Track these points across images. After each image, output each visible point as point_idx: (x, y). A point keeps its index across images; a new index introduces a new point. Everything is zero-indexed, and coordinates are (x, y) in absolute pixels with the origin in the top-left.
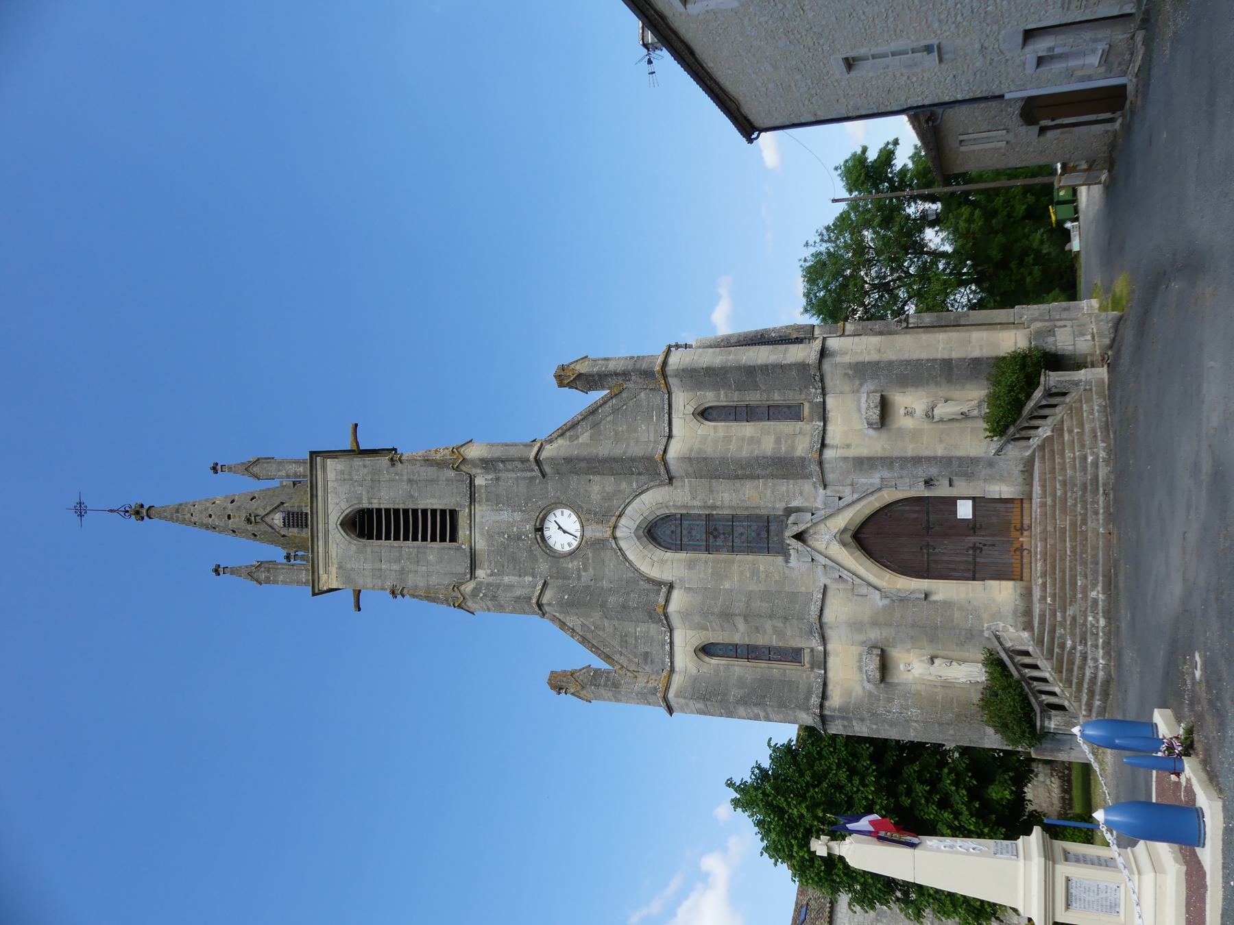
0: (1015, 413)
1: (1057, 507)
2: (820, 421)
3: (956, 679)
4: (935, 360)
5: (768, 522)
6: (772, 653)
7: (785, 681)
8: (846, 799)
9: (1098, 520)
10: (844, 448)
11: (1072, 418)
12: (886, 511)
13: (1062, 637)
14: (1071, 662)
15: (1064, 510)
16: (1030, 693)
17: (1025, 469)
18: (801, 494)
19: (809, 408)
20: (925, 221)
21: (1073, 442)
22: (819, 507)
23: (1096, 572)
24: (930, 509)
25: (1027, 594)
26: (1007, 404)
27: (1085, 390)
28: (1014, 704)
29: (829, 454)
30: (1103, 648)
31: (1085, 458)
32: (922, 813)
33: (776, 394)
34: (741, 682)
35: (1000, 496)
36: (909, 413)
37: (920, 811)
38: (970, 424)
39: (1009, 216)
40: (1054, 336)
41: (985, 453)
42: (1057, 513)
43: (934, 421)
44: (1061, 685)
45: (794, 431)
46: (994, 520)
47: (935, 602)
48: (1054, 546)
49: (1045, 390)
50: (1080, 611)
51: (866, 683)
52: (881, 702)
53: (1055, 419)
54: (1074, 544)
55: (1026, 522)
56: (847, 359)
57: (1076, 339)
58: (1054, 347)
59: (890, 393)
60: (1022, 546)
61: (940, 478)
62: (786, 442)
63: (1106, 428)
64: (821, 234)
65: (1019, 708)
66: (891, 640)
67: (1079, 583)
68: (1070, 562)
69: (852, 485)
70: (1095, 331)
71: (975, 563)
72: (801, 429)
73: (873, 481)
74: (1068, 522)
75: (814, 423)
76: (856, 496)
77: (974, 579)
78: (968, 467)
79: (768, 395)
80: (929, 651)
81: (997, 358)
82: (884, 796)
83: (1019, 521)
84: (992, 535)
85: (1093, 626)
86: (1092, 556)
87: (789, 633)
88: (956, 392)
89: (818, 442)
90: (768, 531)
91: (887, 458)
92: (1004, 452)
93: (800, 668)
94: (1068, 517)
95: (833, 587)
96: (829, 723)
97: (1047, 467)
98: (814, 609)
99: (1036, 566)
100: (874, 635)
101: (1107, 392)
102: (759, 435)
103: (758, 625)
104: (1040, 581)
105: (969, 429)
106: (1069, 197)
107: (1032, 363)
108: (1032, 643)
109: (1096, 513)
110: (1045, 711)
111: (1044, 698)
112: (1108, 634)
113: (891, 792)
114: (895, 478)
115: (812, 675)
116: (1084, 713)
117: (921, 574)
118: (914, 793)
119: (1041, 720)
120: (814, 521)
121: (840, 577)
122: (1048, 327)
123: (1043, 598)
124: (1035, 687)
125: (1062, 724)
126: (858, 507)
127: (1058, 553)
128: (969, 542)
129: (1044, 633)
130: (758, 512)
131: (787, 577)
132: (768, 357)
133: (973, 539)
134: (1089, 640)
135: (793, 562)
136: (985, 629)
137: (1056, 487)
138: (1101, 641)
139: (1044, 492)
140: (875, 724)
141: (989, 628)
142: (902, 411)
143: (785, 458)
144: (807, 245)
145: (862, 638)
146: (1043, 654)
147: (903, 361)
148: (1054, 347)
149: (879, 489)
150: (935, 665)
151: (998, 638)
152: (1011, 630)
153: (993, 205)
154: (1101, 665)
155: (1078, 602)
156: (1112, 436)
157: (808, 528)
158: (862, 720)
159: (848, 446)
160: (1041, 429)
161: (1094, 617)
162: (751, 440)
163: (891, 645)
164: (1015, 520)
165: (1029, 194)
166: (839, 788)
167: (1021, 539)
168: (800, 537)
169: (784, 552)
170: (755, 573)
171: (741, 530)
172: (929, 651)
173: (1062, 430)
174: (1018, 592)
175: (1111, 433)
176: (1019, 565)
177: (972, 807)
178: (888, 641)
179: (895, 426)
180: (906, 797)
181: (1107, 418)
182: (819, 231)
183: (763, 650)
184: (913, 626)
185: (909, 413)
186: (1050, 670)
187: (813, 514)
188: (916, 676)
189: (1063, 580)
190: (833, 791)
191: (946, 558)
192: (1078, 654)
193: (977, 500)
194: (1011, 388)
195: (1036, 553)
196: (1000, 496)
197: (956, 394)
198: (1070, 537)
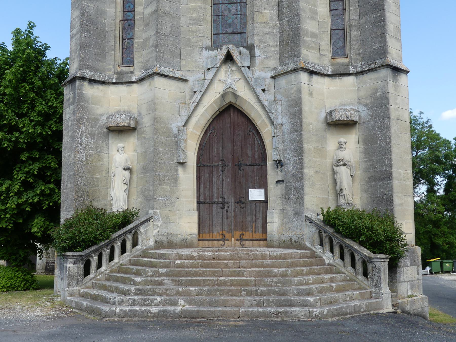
0: (347, 233)
1: (263, 269)
2: (332, 72)
3: (113, 189)
4: (390, 165)
5: (241, 33)
6: (129, 41)
7: (105, 50)
8: (24, 112)
9: (252, 306)
10: (309, 90)
11: (343, 281)
12: (253, 131)
13: (146, 273)
14: (123, 281)
15: (259, 275)
16: (98, 246)
17: (293, 242)
18: (267, 58)
19: (343, 63)
20: (432, 185)
21: (323, 283)
22: (256, 74)
23: (202, 304)
24: (256, 167)
25: (186, 244)
26: (356, 226)
27: (371, 292)
28: (87, 234)
29: (304, 76)
30: (130, 310)
31: (310, 294)
32: (17, 169)
33: (356, 33)
34: (101, 13)
35: (269, 222)
36: (341, 146)
37: (20, 168)
38: (331, 197)
39: (435, 235)
40: (411, 265)
41: (307, 209)
42: (257, 269)
43: (335, 168)
44: (108, 271)
45: (323, 50)
46: (248, 218)
47: (177, 171)
48: (227, 266)
49: (371, 258)
50: (167, 289)
51: (105, 117)
52: (90, 129)
53: (341, 267)
54: (229, 284)
55: (247, 243)
56: (391, 90)
57: (408, 283)
58: (402, 264)
59: (358, 131)
60: (227, 240)
61: (284, 173)
62: (313, 42)
63: (340, 313)
64: (427, 122)
65: (84, 237)
66: (143, 136)
67: (192, 289)
68: (212, 281)
69: (275, 100)
70: (415, 298)
71: (212, 203)
72: (325, 55)
73: (280, 117)
74: (248, 278)
75: (330, 67)
76: (266, 103)
77: (198, 203)
78: (294, 195)
79: (355, 26)
80: (136, 167)
81: (393, 217)
82: (27, 140)
83: (248, 238)
84: (235, 216)
85: (152, 301)
86: (217, 301)
87: (146, 52)
88: (359, 185)
89: (314, 69)
90: (233, 33)
91: (301, 126)
92: (309, 224)
93: (117, 63)
94: (254, 278)
95: (186, 87)
96: (71, 87)
97: (297, 260)
98: (166, 70)
99: (209, 251)
100: (146, 121)
101: (372, 312)
102: (318, 20)
103: (151, 24)
104: (195, 254)
105: (326, 197)
106: (445, 269)
107: (393, 247)
108: (145, 248)
109: (259, 305)
110: (82, 259)
111: (94, 258)
112: (143, 315)
113: (31, 146)
114: (283, 135)
115: (111, 73)
116: (82, 291)
117: (201, 160)
118: (32, 163)
119: (73, 256)
120: (243, 69)
121: (195, 92)
122: (418, 259)
123: (180, 257)
124: (105, 251)
125: (71, 273)
126: (257, 106)
127: (220, 269)
128: (228, 198)
129: (152, 258)
130: (250, 22)
131: (193, 49)
132: (392, 23)
133: (231, 201)
134: (140, 297)
135: (207, 54)
136: (155, 210)
137: (280, 267)
138: (137, 309)
139: (276, 258)
140: (71, 124)
141: (155, 213)
142: (343, 140)
143: (299, 40)
144: (421, 113)
145: (144, 112)
146: (135, 257)
147: (390, 138)
148: (402, 264)
149: (272, 123)
150: (123, 171)
151: (147, 221)
152: (155, 232)
153: (443, 225)
154: (114, 309)
155: (174, 287)
156: (334, 319)
157: (237, 64)
158: (74, 113)
159: (311, 94)
160: (331, 254)
161: (160, 302)
162: (314, 13)
163: (139, 136)
164: (248, 235)
165: (449, 246)
166: (32, 107)
167: (233, 239)
168: (229, 58)
169: (215, 46)
170: (196, 21)
171: (233, 11)
172: (136, 167)
173: (331, 272)
174: (189, 237)
175: (337, 318)
176: (211, 238)
177: (26, 206)
178: (143, 132)
179: (328, 136)
180: (27, 156)
181: (349, 314)
182: (429, 121)
183: (131, 33)
184: (155, 152)
185: (341, 146)
186: (121, 262)
187: (249, 68)
188: (114, 157)
189: (195, 274)
190: (29, 101)
191: (215, 180)
192: (127, 287)
193: (265, 204)
194: (370, 229)
195: (221, 251)
196: (269, 222)
197: (358, 186)
198: (235, 280)
